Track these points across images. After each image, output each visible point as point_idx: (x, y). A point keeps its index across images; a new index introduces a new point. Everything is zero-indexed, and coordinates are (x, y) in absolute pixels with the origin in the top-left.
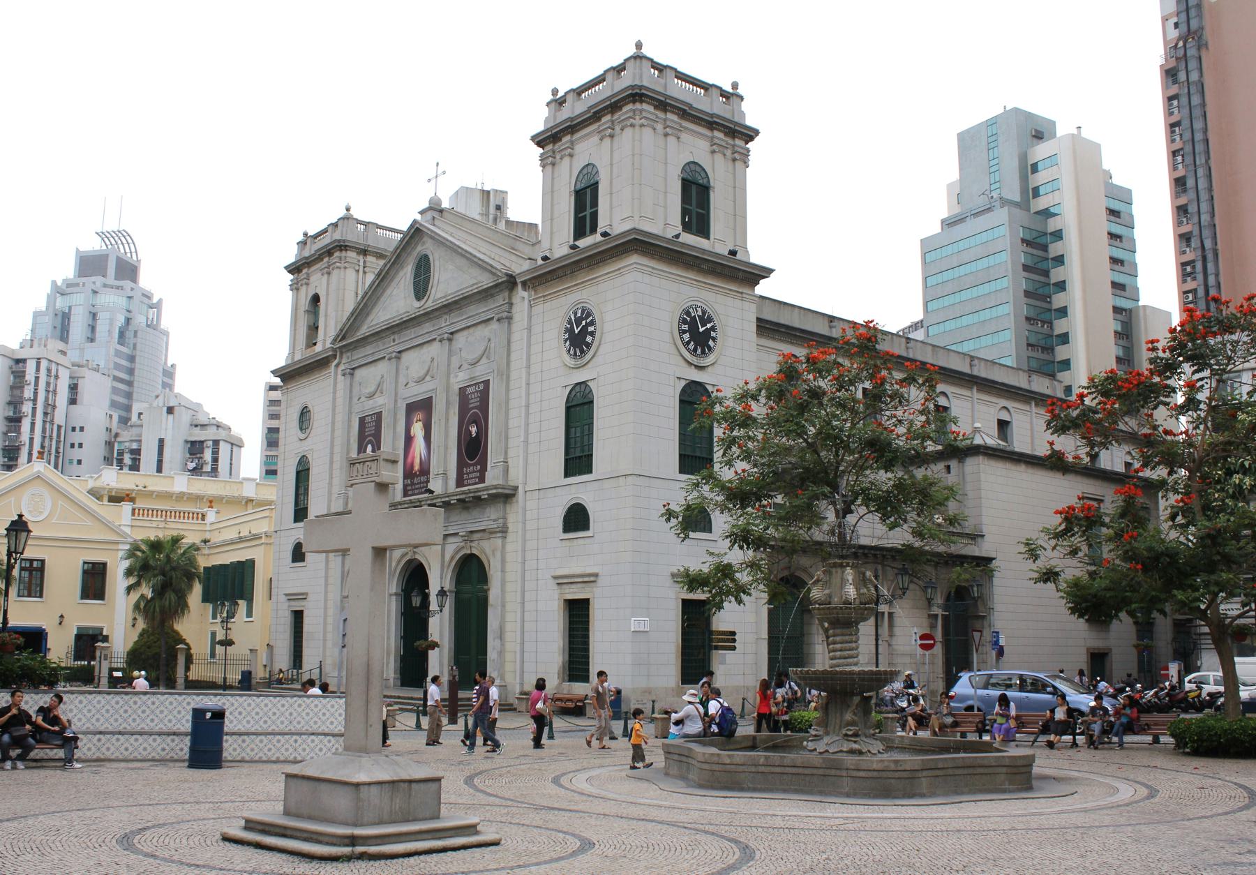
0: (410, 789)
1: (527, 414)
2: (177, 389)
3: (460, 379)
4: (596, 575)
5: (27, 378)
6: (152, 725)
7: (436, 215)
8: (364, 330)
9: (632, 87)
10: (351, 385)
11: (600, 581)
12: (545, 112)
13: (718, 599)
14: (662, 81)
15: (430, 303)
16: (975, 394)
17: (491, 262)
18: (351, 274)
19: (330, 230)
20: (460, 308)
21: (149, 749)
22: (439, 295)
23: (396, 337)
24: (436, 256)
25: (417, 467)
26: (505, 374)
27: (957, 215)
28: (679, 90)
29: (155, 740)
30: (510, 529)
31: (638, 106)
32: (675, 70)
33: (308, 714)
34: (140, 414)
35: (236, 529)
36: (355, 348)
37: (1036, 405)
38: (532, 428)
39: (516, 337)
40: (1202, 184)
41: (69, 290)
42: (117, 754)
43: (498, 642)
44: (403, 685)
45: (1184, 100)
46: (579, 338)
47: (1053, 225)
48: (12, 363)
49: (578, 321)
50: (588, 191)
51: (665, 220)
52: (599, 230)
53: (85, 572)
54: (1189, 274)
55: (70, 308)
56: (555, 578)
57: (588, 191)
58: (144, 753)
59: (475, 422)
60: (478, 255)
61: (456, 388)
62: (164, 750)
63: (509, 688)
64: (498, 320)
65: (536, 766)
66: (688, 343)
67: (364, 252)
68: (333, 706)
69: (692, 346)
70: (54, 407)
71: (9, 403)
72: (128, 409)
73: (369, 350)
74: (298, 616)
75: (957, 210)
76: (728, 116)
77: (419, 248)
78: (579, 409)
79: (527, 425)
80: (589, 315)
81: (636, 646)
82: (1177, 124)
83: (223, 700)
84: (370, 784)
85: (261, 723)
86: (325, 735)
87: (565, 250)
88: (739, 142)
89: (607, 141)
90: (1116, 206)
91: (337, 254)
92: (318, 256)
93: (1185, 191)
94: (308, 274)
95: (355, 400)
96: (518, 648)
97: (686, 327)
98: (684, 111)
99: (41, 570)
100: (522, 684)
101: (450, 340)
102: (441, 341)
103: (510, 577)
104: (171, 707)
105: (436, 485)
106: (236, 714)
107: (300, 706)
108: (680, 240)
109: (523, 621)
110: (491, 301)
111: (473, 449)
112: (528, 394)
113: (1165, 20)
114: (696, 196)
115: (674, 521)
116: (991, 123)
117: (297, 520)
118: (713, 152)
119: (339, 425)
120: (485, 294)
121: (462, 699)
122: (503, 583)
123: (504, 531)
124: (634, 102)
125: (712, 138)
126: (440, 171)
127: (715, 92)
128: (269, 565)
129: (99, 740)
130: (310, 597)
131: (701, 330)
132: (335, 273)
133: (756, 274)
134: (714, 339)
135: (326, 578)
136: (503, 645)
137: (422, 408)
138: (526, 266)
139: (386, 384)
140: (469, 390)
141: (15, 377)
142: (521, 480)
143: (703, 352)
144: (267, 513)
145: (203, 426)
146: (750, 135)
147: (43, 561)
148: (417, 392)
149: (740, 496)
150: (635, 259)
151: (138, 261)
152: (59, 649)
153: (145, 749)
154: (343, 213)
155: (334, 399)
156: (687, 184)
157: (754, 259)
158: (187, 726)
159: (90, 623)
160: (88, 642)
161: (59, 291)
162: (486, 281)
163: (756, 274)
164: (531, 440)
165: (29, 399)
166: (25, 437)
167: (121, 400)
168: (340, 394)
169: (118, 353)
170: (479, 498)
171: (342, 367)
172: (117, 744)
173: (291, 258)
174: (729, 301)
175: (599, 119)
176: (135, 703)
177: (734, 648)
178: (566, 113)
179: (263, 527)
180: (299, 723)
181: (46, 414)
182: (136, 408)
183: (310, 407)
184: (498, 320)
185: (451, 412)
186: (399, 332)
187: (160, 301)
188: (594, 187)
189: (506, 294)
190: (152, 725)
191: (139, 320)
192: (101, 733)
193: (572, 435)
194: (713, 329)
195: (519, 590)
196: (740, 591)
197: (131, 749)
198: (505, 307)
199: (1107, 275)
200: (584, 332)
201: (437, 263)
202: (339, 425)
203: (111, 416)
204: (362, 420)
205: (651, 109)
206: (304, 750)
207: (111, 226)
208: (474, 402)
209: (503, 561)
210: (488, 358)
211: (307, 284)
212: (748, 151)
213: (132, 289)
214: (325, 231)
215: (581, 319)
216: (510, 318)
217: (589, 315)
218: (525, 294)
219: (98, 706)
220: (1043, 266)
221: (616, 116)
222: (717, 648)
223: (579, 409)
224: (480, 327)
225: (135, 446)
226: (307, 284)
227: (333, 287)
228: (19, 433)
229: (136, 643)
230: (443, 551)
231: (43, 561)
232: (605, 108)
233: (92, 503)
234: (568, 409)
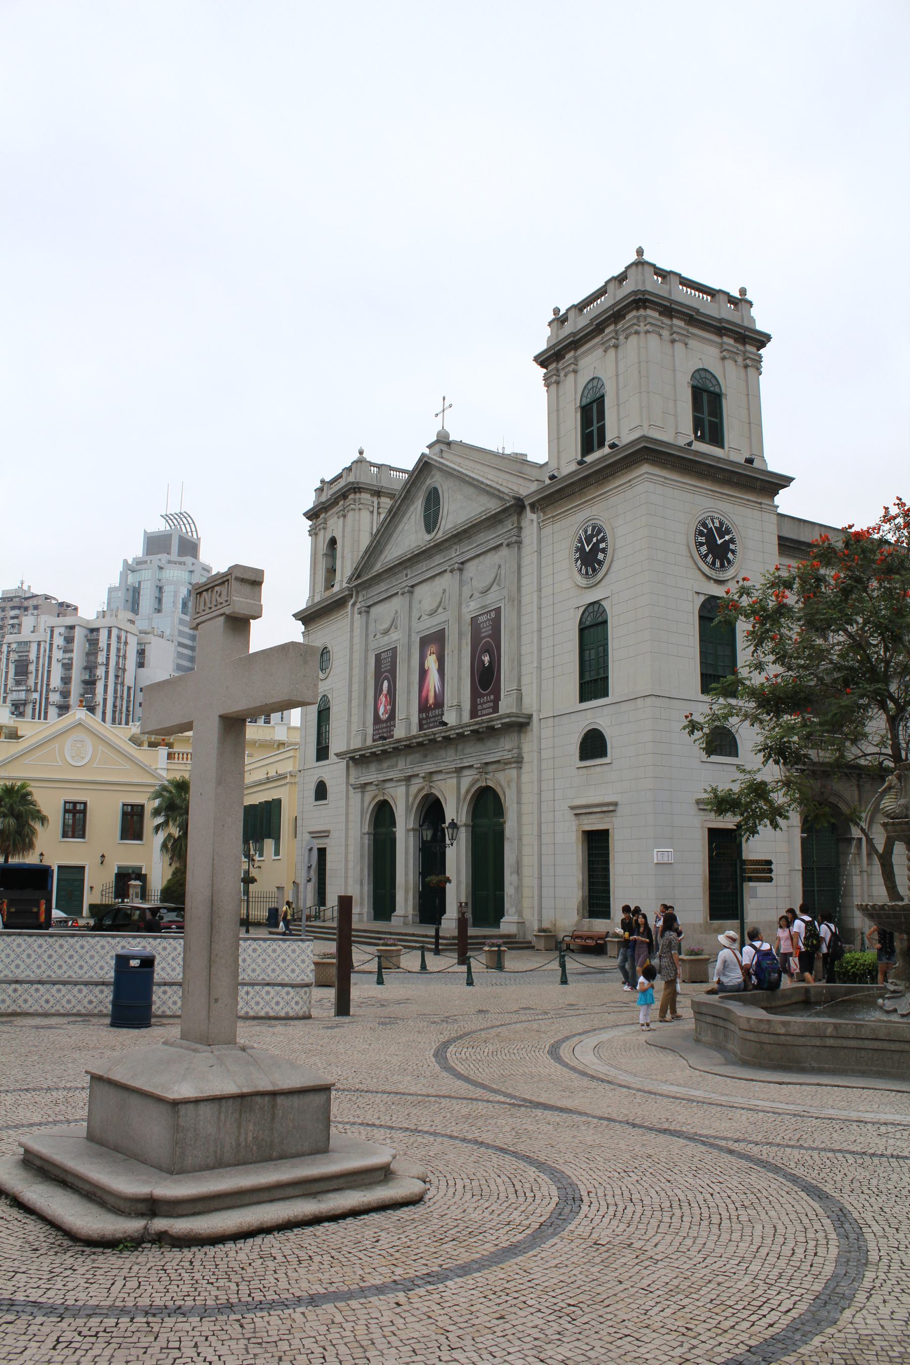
0: (274, 1106)
1: (540, 639)
3: (471, 608)
4: (616, 804)
5: (100, 645)
6: (81, 972)
7: (444, 447)
8: (378, 567)
9: (635, 293)
10: (367, 623)
11: (620, 810)
12: (548, 331)
13: (751, 823)
14: (666, 287)
15: (440, 534)
17: (498, 487)
18: (365, 514)
19: (344, 475)
20: (469, 537)
21: (74, 1002)
22: (449, 526)
23: (409, 571)
24: (445, 488)
25: (431, 701)
26: (516, 600)
29: (80, 991)
30: (526, 760)
32: (679, 275)
33: (264, 960)
35: (264, 770)
36: (370, 586)
38: (545, 654)
39: (526, 561)
41: (139, 567)
42: (36, 1008)
43: (515, 877)
44: (421, 922)
46: (591, 556)
48: (87, 632)
49: (589, 539)
50: (595, 405)
51: (677, 427)
52: (607, 443)
53: (124, 814)
55: (140, 582)
56: (572, 808)
57: (595, 405)
58: (68, 1006)
59: (487, 651)
60: (485, 481)
61: (467, 618)
62: (91, 1002)
63: (527, 924)
64: (508, 545)
65: (535, 1026)
66: (706, 556)
67: (378, 493)
68: (294, 951)
69: (710, 559)
70: (124, 670)
71: (85, 668)
73: (383, 586)
76: (738, 321)
77: (428, 482)
78: (593, 631)
79: (540, 650)
80: (600, 531)
81: (661, 870)
83: (154, 943)
84: (197, 1101)
86: (283, 985)
87: (573, 467)
88: (750, 348)
89: (612, 352)
91: (351, 496)
92: (334, 500)
94: (325, 519)
95: (371, 637)
96: (536, 882)
98: (691, 316)
99: (84, 812)
100: (540, 921)
101: (461, 570)
102: (451, 571)
103: (525, 809)
104: (102, 952)
105: (450, 718)
107: (255, 950)
108: (693, 448)
109: (540, 855)
110: (500, 527)
111: (486, 679)
112: (540, 620)
114: (707, 403)
115: (698, 734)
117: (319, 758)
119: (356, 663)
120: (493, 521)
121: (472, 937)
122: (519, 815)
123: (519, 761)
124: (638, 309)
125: (722, 344)
126: (447, 405)
127: (722, 299)
128: (295, 803)
129: (15, 990)
130: (332, 835)
131: (719, 542)
132: (350, 515)
133: (774, 484)
134: (733, 552)
135: (347, 814)
136: (520, 880)
137: (435, 640)
138: (534, 487)
139: (398, 619)
140: (482, 619)
141: (90, 644)
142: (535, 708)
143: (722, 565)
144: (291, 754)
146: (762, 340)
147: (85, 804)
148: (429, 625)
149: (773, 701)
150: (646, 468)
151: (199, 539)
152: (97, 889)
153: (69, 1001)
154: (356, 456)
155: (352, 638)
156: (698, 393)
157: (772, 467)
158: (110, 975)
159: (130, 862)
160: (126, 879)
161: (130, 568)
162: (494, 506)
163: (774, 484)
164: (544, 665)
165: (102, 664)
166: (99, 698)
168: (357, 632)
169: (181, 622)
170: (492, 728)
171: (358, 605)
172: (36, 995)
173: (309, 502)
174: (748, 512)
175: (602, 331)
176: (61, 946)
177: (770, 880)
178: (568, 328)
179: (287, 767)
180: (254, 970)
181: (117, 677)
183: (330, 648)
184: (508, 545)
185: (464, 642)
186: (411, 567)
189: (515, 518)
190: (81, 972)
192: (17, 982)
193: (587, 658)
194: (732, 541)
195: (536, 822)
196: (775, 814)
197: (52, 1001)
200: (595, 549)
201: (446, 495)
202: (356, 663)
204: (378, 657)
205: (656, 315)
206: (258, 1003)
207: (174, 509)
208: (486, 631)
209: (519, 792)
210: (499, 585)
211: (325, 529)
212: (760, 357)
213: (193, 564)
214: (340, 476)
215: (592, 536)
216: (519, 543)
218: (534, 516)
219: (18, 950)
221: (619, 326)
222: (750, 879)
223: (593, 631)
224: (489, 555)
226: (325, 529)
227: (348, 529)
228: (94, 694)
229: (169, 881)
230: (459, 784)
231: (85, 804)
232: (608, 318)
233: (132, 749)
234: (582, 631)
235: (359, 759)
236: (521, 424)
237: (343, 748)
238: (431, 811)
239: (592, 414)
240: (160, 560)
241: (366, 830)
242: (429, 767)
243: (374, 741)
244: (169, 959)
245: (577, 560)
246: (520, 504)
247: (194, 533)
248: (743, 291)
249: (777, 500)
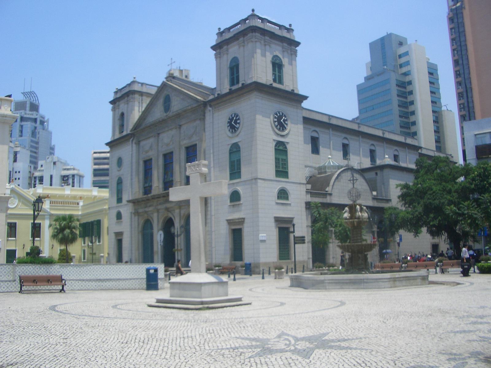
3: (186, 142)
4: (244, 219)
8: (143, 126)
11: (246, 221)
12: (216, 37)
15: (170, 114)
16: (385, 145)
26: (201, 140)
27: (370, 76)
28: (268, 27)
31: (254, 34)
34: (42, 166)
37: (408, 148)
40: (465, 62)
45: (457, 30)
46: (233, 124)
66: (277, 126)
74: (119, 242)
75: (370, 73)
85: (80, 286)
88: (293, 47)
90: (431, 71)
92: (123, 97)
97: (276, 120)
106: (122, 271)
114: (277, 66)
118: (283, 51)
146: (298, 44)
187: (48, 120)
188: (237, 66)
190: (90, 277)
203: (31, 167)
207: (28, 90)
212: (297, 50)
217: (237, 116)
221: (246, 38)
235: (134, 202)
236: (206, 73)
239: (234, 70)
240: (21, 113)
243: (32, 194)
244: (118, 272)
245: (228, 126)
246: (206, 103)
247: (37, 101)
248: (290, 25)
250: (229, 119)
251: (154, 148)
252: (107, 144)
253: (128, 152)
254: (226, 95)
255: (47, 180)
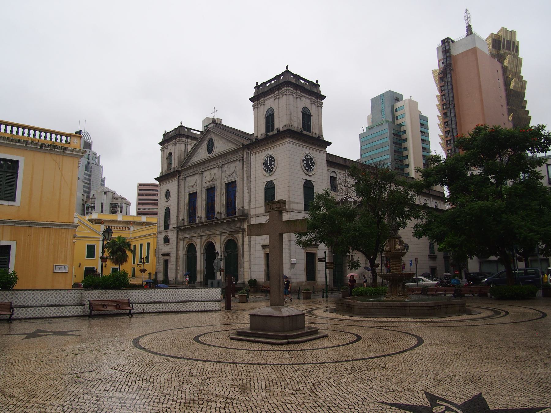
2: (106, 186)
3: (226, 180)
8: (189, 164)
12: (254, 90)
34: (93, 195)
46: (269, 165)
47: (403, 129)
54: (449, 144)
69: (307, 168)
72: (89, 193)
74: (166, 263)
75: (371, 124)
77: (209, 136)
82: (444, 95)
90: (423, 122)
92: (168, 139)
93: (447, 117)
95: (186, 188)
97: (305, 162)
113: (439, 61)
114: (306, 116)
116: (382, 95)
118: (312, 104)
130: (171, 255)
139: (197, 183)
145: (117, 198)
146: (323, 97)
154: (180, 125)
167: (86, 190)
182: (92, 192)
187: (100, 156)
191: (92, 162)
198: (242, 156)
199: (420, 145)
200: (271, 164)
217: (272, 158)
220: (400, 142)
225: (92, 205)
227: (177, 150)
233: (90, 224)
235: (179, 229)
237: (175, 226)
238: (210, 248)
239: (270, 118)
241: (185, 253)
242: (210, 232)
248: (317, 81)
249: (327, 150)
250: (265, 160)
251: (197, 183)
252: (156, 179)
253: (172, 186)
254: (262, 140)
255: (98, 207)
